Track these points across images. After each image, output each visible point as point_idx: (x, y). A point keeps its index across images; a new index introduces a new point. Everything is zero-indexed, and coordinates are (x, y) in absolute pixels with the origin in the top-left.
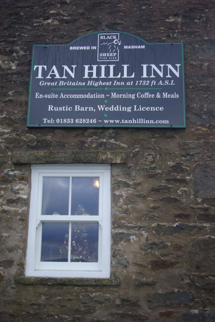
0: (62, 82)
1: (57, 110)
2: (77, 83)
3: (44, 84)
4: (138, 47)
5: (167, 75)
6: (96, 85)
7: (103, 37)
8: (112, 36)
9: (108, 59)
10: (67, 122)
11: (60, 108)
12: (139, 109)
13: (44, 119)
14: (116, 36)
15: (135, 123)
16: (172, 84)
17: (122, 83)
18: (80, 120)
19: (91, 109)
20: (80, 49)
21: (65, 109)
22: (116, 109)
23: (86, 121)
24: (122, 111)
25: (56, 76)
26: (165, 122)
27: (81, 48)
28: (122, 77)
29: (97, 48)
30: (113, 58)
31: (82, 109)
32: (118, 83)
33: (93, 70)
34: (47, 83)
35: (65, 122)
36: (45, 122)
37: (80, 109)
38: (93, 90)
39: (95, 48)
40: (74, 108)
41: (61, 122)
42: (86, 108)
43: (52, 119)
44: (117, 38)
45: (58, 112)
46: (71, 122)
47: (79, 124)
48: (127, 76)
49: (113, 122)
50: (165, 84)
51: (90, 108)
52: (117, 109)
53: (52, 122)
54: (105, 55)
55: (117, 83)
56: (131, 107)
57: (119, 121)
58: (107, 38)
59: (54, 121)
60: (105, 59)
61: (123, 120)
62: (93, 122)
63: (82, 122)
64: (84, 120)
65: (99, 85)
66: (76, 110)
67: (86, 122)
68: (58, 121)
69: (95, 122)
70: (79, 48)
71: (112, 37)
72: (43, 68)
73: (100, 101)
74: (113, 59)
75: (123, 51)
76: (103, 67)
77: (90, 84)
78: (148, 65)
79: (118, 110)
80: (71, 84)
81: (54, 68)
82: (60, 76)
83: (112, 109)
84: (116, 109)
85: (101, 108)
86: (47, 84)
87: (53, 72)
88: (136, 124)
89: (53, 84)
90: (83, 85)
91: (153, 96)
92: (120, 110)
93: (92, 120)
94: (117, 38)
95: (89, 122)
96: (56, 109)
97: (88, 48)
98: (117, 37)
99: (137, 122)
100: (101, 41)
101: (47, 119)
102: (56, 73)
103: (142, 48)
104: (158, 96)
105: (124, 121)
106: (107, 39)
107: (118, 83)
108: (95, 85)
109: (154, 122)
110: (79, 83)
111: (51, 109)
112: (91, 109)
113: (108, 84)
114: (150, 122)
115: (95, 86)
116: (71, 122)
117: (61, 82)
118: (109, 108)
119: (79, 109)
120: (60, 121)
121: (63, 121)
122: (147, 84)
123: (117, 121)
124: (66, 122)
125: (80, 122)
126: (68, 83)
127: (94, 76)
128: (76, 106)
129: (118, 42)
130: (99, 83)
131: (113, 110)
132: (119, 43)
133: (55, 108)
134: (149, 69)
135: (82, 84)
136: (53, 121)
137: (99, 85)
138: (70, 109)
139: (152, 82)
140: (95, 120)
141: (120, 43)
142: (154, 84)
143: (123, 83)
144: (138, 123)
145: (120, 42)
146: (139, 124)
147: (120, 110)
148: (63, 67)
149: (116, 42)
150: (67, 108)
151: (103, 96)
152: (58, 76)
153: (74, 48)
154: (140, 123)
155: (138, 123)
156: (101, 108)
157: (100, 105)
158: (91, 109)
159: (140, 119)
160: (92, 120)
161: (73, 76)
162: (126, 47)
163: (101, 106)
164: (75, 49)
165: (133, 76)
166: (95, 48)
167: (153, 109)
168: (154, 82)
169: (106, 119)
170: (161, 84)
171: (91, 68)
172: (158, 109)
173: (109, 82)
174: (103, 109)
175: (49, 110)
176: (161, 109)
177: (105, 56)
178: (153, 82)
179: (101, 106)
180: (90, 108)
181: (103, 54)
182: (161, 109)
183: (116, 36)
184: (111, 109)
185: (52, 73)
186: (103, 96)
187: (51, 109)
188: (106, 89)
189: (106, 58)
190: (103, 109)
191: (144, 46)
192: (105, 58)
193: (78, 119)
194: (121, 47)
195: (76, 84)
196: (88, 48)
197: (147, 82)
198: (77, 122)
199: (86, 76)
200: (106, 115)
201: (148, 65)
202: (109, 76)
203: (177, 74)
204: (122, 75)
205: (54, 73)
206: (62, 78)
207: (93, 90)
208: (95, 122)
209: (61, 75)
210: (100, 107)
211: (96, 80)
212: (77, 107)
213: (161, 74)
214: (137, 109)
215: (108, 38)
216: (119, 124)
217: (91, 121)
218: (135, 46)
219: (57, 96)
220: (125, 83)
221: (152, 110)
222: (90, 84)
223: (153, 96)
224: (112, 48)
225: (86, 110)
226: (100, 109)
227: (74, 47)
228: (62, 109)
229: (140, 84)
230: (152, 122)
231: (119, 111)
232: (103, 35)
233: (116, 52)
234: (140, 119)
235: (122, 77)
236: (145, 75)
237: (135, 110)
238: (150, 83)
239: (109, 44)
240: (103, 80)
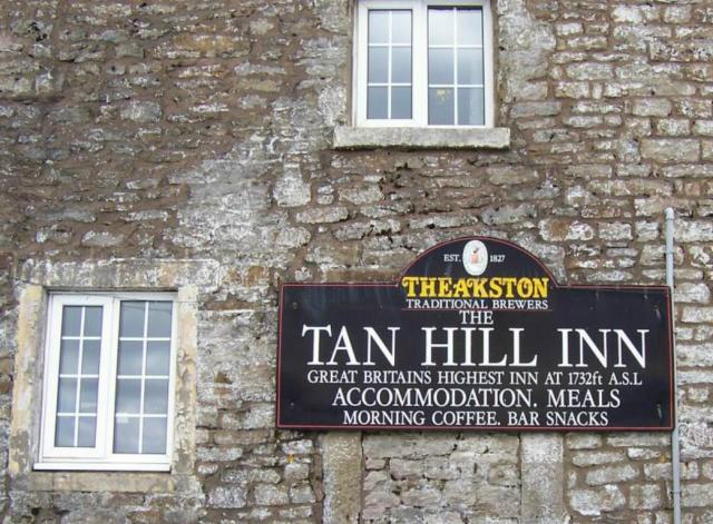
33: (446, 343)
48: (490, 361)
82: (358, 360)
134: (574, 338)
148: (366, 332)
161: (613, 375)
165: (534, 363)
203: (536, 381)
204: (511, 360)
236: (565, 363)
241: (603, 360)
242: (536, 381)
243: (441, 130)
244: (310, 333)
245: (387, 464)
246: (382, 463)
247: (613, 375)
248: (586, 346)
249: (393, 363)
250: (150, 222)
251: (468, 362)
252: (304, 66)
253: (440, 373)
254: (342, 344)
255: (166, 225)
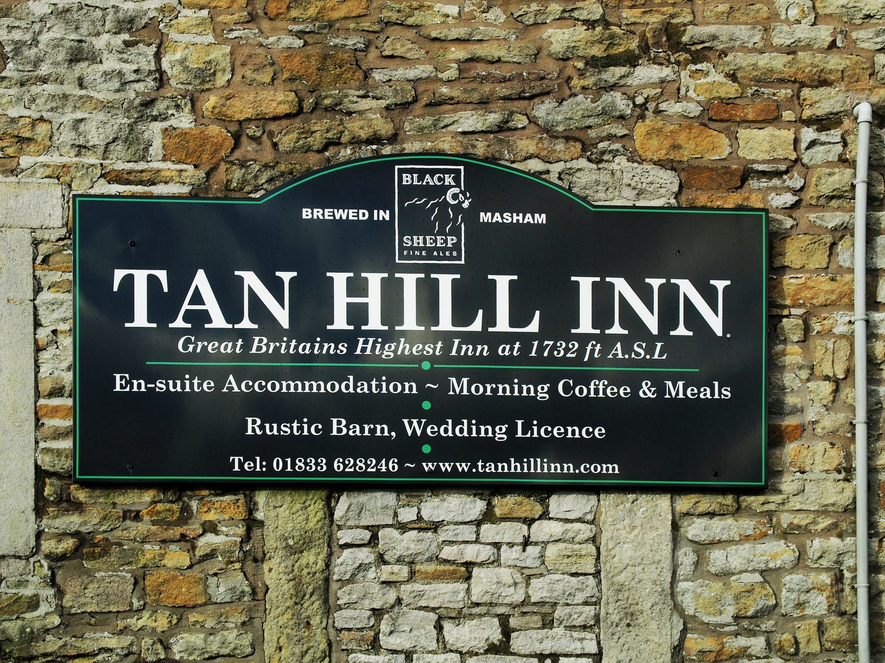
0: (261, 341)
1: (275, 432)
2: (317, 345)
3: (195, 348)
4: (524, 219)
5: (675, 326)
6: (388, 353)
7: (412, 179)
8: (442, 176)
9: (430, 257)
10: (308, 468)
11: (282, 427)
12: (532, 433)
13: (232, 458)
14: (452, 175)
15: (519, 470)
16: (656, 357)
17: (479, 348)
18: (347, 462)
19: (382, 430)
20: (338, 217)
21: (300, 428)
22: (461, 431)
23: (367, 466)
24: (478, 438)
25: (210, 321)
26: (607, 469)
27: (341, 214)
28: (490, 329)
29: (392, 215)
30: (447, 253)
32: (468, 350)
33: (366, 295)
34: (206, 344)
35: (300, 467)
36: (236, 469)
37: (349, 429)
39: (387, 218)
40: (328, 427)
41: (289, 469)
42: (366, 427)
43: (258, 458)
44: (459, 186)
46: (319, 468)
47: (344, 474)
49: (449, 469)
50: (633, 356)
51: (379, 427)
52: (463, 430)
53: (258, 469)
54: (418, 241)
55: (464, 347)
56: (507, 426)
57: (469, 464)
58: (425, 181)
59: (264, 463)
60: (421, 258)
61: (480, 464)
62: (388, 469)
63: (355, 469)
64: (361, 461)
65: (399, 353)
66: (335, 433)
67: (367, 468)
69: (393, 467)
70: (333, 212)
71: (440, 179)
72: (153, 282)
74: (445, 258)
75: (477, 231)
76: (410, 281)
77: (364, 350)
78: (598, 279)
79: (465, 434)
80: (296, 347)
81: (201, 280)
84: (461, 431)
86: (204, 348)
87: (197, 298)
88: (522, 475)
89: (226, 347)
90: (338, 351)
92: (474, 434)
93: (384, 461)
94: (459, 186)
95: (377, 468)
96: (271, 429)
97: (363, 215)
98: (457, 179)
99: (522, 468)
100: (407, 192)
101: (242, 458)
102: (211, 304)
103: (536, 222)
105: (484, 467)
106: (424, 183)
107: (468, 350)
108: (382, 353)
109: (574, 470)
110: (326, 346)
111: (254, 430)
112: (383, 430)
113: (429, 349)
114: (562, 468)
115: (383, 356)
116: (319, 468)
117: (257, 339)
118: (439, 429)
119: (345, 431)
120: (285, 464)
121: (293, 464)
122: (569, 355)
124: (303, 466)
125: (347, 470)
126: (284, 345)
127: (375, 322)
128: (335, 421)
129: (461, 195)
130: (397, 348)
131: (450, 434)
132: (464, 202)
133: (267, 426)
134: (603, 294)
135: (336, 348)
136: (261, 466)
137: (399, 353)
138: (317, 430)
139: (589, 348)
140: (393, 462)
141: (466, 201)
142: (596, 356)
143: (483, 350)
144: (526, 471)
145: (468, 199)
146: (528, 475)
147: (474, 434)
148: (241, 279)
149: (455, 196)
150: (305, 426)
152: (218, 321)
153: (318, 213)
154: (532, 471)
155: (526, 471)
156: (413, 427)
157: (410, 417)
158: (383, 430)
159: (532, 460)
160: (384, 461)
163: (415, 421)
164: (321, 217)
166: (387, 218)
167: (574, 432)
168: (596, 346)
169: (428, 458)
170: (620, 356)
171: (357, 287)
172: (588, 433)
173: (435, 343)
174: (419, 433)
175: (250, 432)
176: (598, 432)
177: (421, 245)
178: (593, 345)
179: (415, 421)
180: (379, 427)
181: (412, 240)
182: (598, 432)
183: (452, 175)
184: (446, 431)
185: (190, 304)
187: (254, 430)
188: (426, 366)
189: (424, 253)
190: (419, 433)
191: (544, 216)
192: (421, 253)
193: (341, 460)
194: (471, 216)
195: (312, 347)
196: (364, 215)
197: (571, 346)
198: (339, 467)
199: (340, 322)
200: (426, 449)
201: (598, 279)
202: (437, 323)
203: (716, 323)
204: (490, 319)
205: (203, 304)
206: (236, 326)
208: (393, 467)
210: (411, 424)
212: (339, 423)
213: (651, 322)
214: (524, 432)
215: (428, 183)
216: (469, 474)
217: (381, 466)
218: (515, 215)
220: (493, 350)
221: (570, 436)
222: (364, 350)
225: (367, 433)
226: (410, 432)
227: (315, 210)
228: (291, 428)
229: (546, 354)
230: (569, 468)
231: (470, 438)
232: (411, 171)
233: (455, 232)
234: (532, 460)
235: (490, 329)
236: (586, 325)
237: (520, 435)
238: (581, 351)
239: (432, 202)
241: (651, 322)
242: (716, 323)
245: (374, 538)
246: (367, 535)
248: (624, 302)
249: (285, 323)
253: (361, 340)
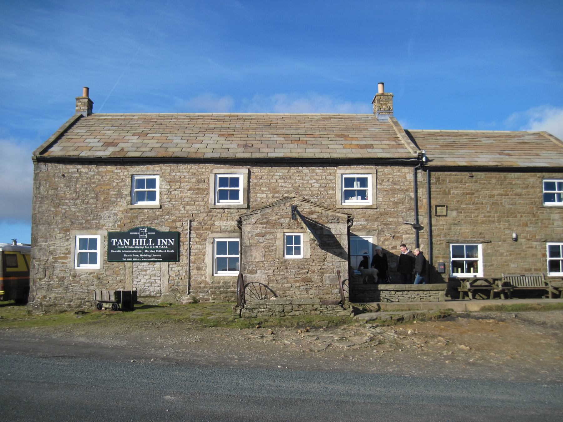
31: (135, 256)
32: (147, 247)
38: (137, 249)
45: (127, 257)
52: (146, 256)
54: (142, 236)
68: (127, 259)
73: (140, 253)
75: (148, 235)
81: (120, 240)
83: (145, 256)
85: (141, 255)
91: (163, 251)
100: (141, 231)
102: (121, 243)
104: (165, 251)
107: (147, 247)
112: (138, 256)
123: (146, 259)
127: (137, 244)
134: (161, 241)
143: (148, 247)
151: (141, 251)
156: (141, 255)
158: (138, 256)
162: (149, 233)
165: (154, 245)
167: (158, 256)
171: (136, 241)
176: (160, 256)
186: (141, 251)
194: (147, 233)
203: (173, 244)
204: (149, 244)
207: (137, 249)
209: (123, 244)
211: (139, 246)
213: (166, 244)
219: (121, 251)
223: (163, 251)
224: (145, 233)
236: (159, 244)
240: (141, 246)
242: (173, 244)
243: (546, 251)
244: (113, 241)
247: (173, 245)
250: (95, 223)
251: (141, 244)
252: (123, 193)
254: (120, 242)
255: (98, 224)
